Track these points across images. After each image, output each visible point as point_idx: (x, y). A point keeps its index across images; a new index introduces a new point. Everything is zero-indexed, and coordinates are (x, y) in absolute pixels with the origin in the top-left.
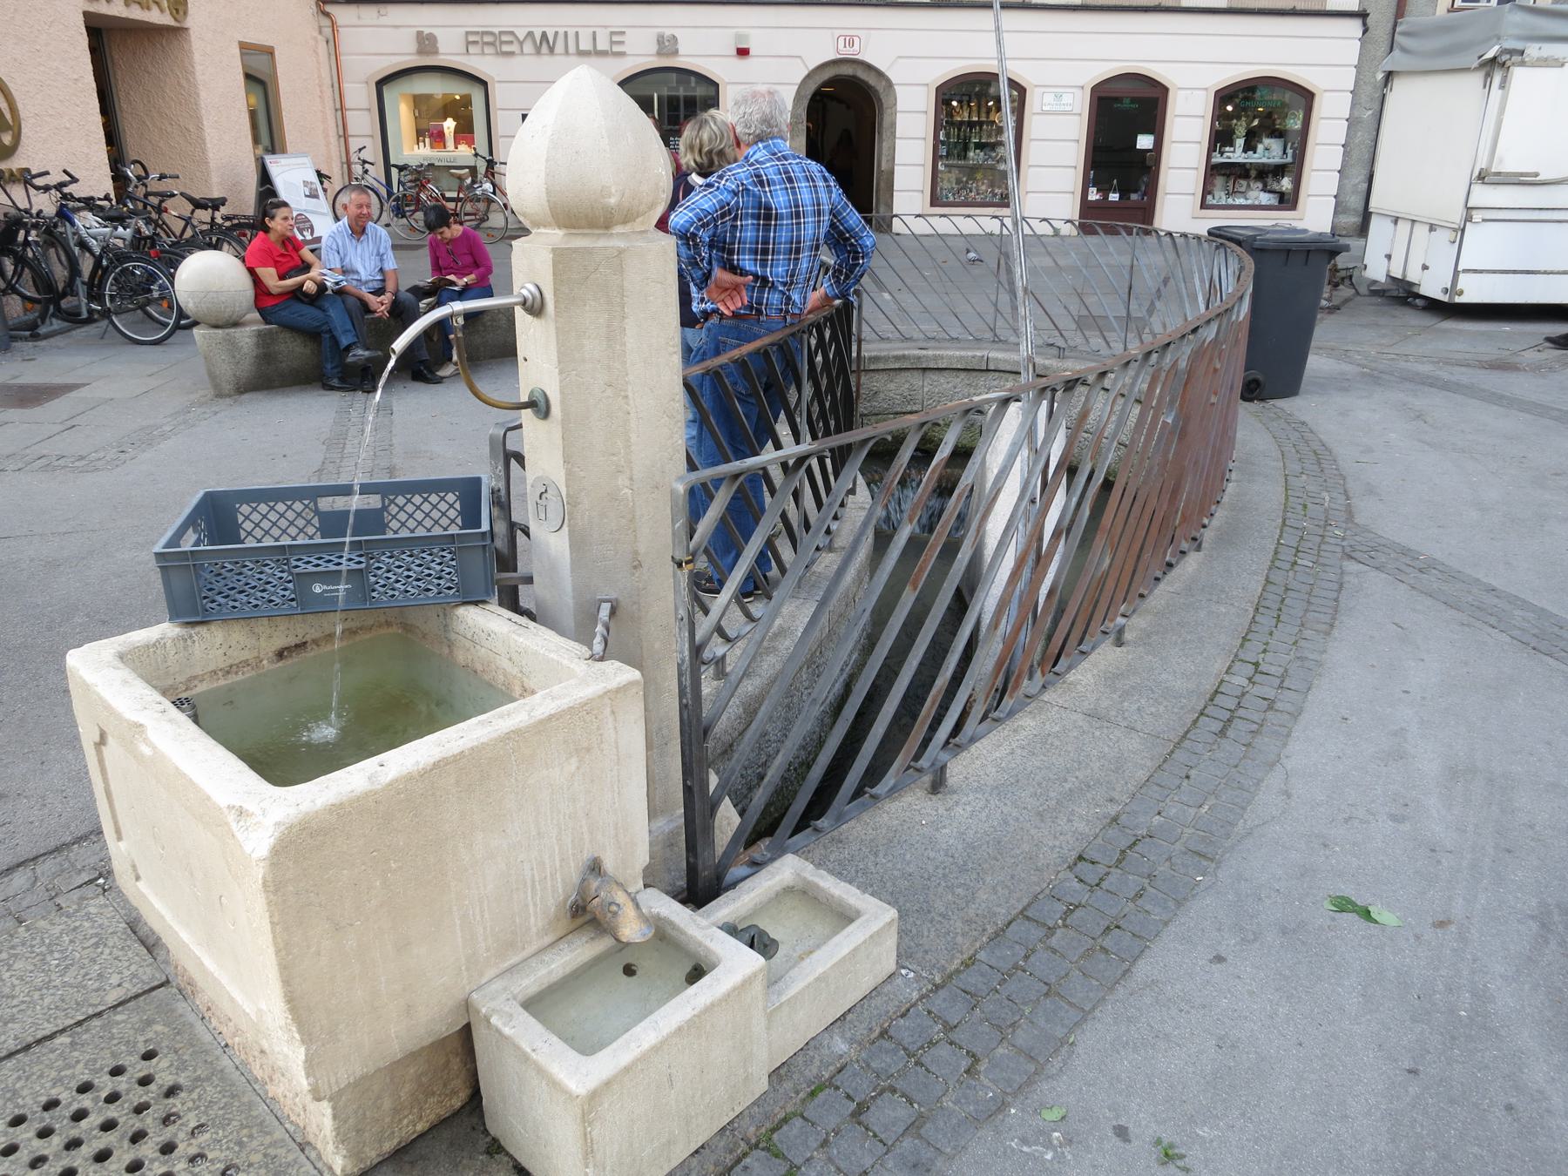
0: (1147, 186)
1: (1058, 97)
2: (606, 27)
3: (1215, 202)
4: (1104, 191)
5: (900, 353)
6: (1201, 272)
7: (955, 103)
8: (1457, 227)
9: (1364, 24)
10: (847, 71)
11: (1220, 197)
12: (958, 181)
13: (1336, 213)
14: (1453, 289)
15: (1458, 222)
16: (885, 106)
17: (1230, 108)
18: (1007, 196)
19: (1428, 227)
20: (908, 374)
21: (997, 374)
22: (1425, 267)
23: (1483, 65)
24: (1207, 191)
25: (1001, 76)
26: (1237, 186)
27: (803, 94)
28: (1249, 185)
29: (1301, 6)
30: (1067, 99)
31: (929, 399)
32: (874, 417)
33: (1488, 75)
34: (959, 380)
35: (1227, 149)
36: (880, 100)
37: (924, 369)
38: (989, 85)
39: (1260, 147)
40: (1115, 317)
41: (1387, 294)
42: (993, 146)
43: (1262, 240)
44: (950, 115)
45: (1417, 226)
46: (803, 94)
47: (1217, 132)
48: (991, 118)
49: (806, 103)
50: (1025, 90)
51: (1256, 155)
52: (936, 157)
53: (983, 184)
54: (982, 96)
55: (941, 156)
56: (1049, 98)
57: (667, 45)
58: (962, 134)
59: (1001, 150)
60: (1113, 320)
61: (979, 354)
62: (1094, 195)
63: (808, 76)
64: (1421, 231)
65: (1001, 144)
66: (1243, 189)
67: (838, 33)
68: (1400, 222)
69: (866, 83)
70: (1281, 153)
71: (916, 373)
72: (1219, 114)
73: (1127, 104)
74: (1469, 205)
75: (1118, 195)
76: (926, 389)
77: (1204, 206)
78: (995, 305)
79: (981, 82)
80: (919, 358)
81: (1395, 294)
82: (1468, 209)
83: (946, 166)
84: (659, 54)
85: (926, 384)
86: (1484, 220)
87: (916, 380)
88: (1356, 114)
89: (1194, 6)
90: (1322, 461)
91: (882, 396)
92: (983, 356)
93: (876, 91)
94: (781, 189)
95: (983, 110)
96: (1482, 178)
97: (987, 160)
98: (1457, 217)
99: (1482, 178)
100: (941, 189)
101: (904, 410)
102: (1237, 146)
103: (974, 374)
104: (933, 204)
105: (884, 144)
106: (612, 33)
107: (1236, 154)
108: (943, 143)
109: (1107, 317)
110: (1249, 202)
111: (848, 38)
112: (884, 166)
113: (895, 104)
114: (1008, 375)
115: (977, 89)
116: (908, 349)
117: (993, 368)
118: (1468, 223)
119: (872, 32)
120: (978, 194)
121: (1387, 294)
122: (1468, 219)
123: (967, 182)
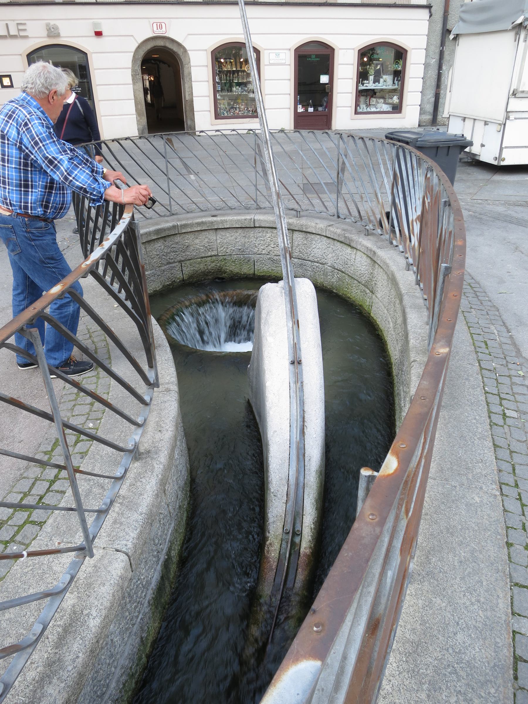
0: (327, 103)
1: (278, 55)
2: (14, 20)
3: (361, 110)
4: (306, 106)
5: (199, 220)
6: (385, 164)
7: (222, 60)
8: (501, 123)
9: (430, 12)
10: (160, 43)
11: (363, 108)
12: (229, 104)
13: (420, 114)
14: (500, 158)
15: (502, 120)
16: (184, 63)
17: (365, 59)
18: (256, 111)
19: (483, 123)
20: (206, 233)
21: (261, 229)
22: (483, 145)
23: (514, 28)
24: (357, 105)
25: (247, 45)
26: (371, 101)
27: (137, 57)
28: (377, 101)
29: (398, 2)
30: (282, 56)
31: (221, 247)
32: (188, 262)
33: (518, 34)
34: (238, 234)
35: (365, 82)
36: (181, 60)
37: (216, 229)
38: (240, 49)
39: (381, 80)
40: (324, 183)
41: (462, 161)
42: (245, 84)
43: (422, 141)
44: (220, 67)
45: (476, 122)
46: (137, 57)
47: (361, 72)
48: (243, 69)
49: (139, 63)
50: (259, 52)
51: (380, 85)
52: (215, 92)
53: (242, 105)
54: (237, 56)
55: (218, 91)
56: (273, 56)
57: (52, 31)
58: (228, 78)
59: (250, 87)
60: (323, 184)
61: (248, 217)
62: (300, 109)
63: (139, 47)
64: (479, 125)
65: (249, 82)
66: (374, 103)
67: (152, 21)
68: (466, 120)
69: (172, 50)
70: (392, 83)
71: (211, 232)
72: (361, 64)
73: (313, 58)
74: (508, 110)
75: (312, 109)
76: (218, 241)
77: (356, 113)
78: (256, 186)
79: (235, 48)
80: (212, 223)
81: (466, 160)
82: (507, 112)
83: (221, 96)
84: (49, 36)
85: (218, 238)
86: (515, 119)
87: (212, 236)
88: (428, 61)
89: (344, 2)
90: (478, 294)
91: (192, 248)
92: (251, 219)
93: (178, 55)
94: (50, 143)
95: (238, 65)
96: (514, 94)
97: (243, 92)
98: (501, 117)
99: (514, 94)
100: (220, 109)
101: (206, 255)
102: (370, 80)
103: (247, 230)
104: (216, 118)
105: (186, 85)
106: (18, 24)
107: (370, 85)
108: (218, 83)
109: (320, 184)
110: (378, 110)
111: (158, 24)
112: (187, 98)
113: (190, 62)
114: (267, 229)
115: (234, 52)
116: (205, 216)
117: (258, 226)
118: (507, 121)
119: (172, 20)
120: (240, 111)
121: (462, 161)
122: (507, 118)
123: (233, 104)
